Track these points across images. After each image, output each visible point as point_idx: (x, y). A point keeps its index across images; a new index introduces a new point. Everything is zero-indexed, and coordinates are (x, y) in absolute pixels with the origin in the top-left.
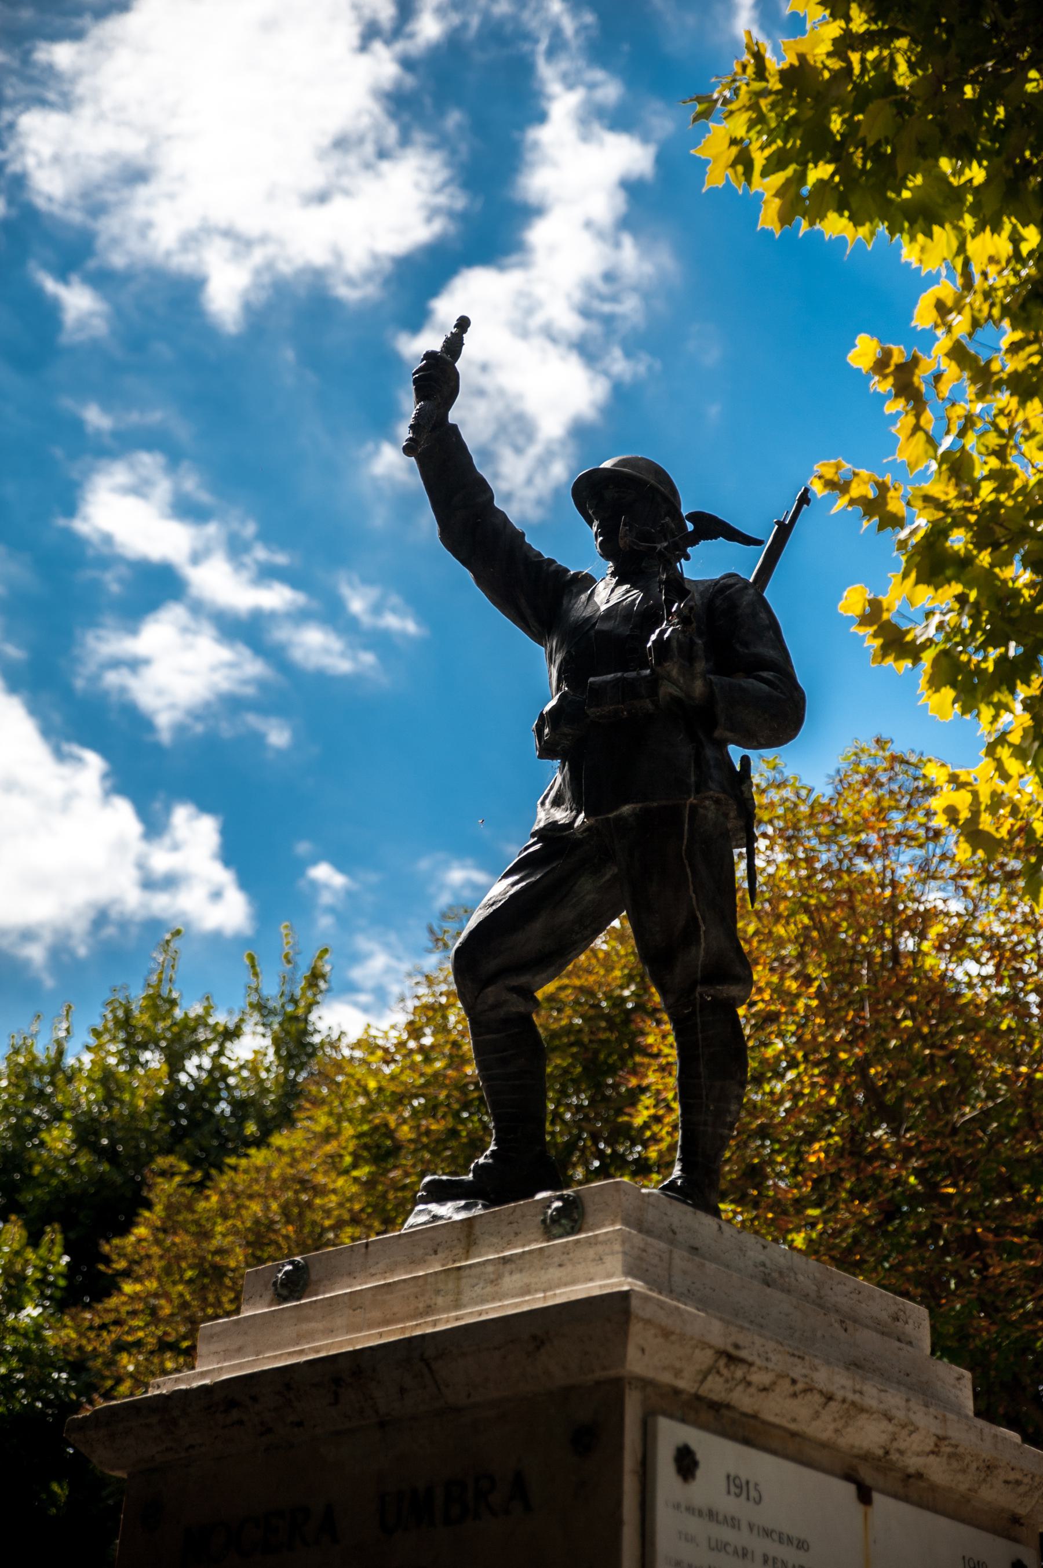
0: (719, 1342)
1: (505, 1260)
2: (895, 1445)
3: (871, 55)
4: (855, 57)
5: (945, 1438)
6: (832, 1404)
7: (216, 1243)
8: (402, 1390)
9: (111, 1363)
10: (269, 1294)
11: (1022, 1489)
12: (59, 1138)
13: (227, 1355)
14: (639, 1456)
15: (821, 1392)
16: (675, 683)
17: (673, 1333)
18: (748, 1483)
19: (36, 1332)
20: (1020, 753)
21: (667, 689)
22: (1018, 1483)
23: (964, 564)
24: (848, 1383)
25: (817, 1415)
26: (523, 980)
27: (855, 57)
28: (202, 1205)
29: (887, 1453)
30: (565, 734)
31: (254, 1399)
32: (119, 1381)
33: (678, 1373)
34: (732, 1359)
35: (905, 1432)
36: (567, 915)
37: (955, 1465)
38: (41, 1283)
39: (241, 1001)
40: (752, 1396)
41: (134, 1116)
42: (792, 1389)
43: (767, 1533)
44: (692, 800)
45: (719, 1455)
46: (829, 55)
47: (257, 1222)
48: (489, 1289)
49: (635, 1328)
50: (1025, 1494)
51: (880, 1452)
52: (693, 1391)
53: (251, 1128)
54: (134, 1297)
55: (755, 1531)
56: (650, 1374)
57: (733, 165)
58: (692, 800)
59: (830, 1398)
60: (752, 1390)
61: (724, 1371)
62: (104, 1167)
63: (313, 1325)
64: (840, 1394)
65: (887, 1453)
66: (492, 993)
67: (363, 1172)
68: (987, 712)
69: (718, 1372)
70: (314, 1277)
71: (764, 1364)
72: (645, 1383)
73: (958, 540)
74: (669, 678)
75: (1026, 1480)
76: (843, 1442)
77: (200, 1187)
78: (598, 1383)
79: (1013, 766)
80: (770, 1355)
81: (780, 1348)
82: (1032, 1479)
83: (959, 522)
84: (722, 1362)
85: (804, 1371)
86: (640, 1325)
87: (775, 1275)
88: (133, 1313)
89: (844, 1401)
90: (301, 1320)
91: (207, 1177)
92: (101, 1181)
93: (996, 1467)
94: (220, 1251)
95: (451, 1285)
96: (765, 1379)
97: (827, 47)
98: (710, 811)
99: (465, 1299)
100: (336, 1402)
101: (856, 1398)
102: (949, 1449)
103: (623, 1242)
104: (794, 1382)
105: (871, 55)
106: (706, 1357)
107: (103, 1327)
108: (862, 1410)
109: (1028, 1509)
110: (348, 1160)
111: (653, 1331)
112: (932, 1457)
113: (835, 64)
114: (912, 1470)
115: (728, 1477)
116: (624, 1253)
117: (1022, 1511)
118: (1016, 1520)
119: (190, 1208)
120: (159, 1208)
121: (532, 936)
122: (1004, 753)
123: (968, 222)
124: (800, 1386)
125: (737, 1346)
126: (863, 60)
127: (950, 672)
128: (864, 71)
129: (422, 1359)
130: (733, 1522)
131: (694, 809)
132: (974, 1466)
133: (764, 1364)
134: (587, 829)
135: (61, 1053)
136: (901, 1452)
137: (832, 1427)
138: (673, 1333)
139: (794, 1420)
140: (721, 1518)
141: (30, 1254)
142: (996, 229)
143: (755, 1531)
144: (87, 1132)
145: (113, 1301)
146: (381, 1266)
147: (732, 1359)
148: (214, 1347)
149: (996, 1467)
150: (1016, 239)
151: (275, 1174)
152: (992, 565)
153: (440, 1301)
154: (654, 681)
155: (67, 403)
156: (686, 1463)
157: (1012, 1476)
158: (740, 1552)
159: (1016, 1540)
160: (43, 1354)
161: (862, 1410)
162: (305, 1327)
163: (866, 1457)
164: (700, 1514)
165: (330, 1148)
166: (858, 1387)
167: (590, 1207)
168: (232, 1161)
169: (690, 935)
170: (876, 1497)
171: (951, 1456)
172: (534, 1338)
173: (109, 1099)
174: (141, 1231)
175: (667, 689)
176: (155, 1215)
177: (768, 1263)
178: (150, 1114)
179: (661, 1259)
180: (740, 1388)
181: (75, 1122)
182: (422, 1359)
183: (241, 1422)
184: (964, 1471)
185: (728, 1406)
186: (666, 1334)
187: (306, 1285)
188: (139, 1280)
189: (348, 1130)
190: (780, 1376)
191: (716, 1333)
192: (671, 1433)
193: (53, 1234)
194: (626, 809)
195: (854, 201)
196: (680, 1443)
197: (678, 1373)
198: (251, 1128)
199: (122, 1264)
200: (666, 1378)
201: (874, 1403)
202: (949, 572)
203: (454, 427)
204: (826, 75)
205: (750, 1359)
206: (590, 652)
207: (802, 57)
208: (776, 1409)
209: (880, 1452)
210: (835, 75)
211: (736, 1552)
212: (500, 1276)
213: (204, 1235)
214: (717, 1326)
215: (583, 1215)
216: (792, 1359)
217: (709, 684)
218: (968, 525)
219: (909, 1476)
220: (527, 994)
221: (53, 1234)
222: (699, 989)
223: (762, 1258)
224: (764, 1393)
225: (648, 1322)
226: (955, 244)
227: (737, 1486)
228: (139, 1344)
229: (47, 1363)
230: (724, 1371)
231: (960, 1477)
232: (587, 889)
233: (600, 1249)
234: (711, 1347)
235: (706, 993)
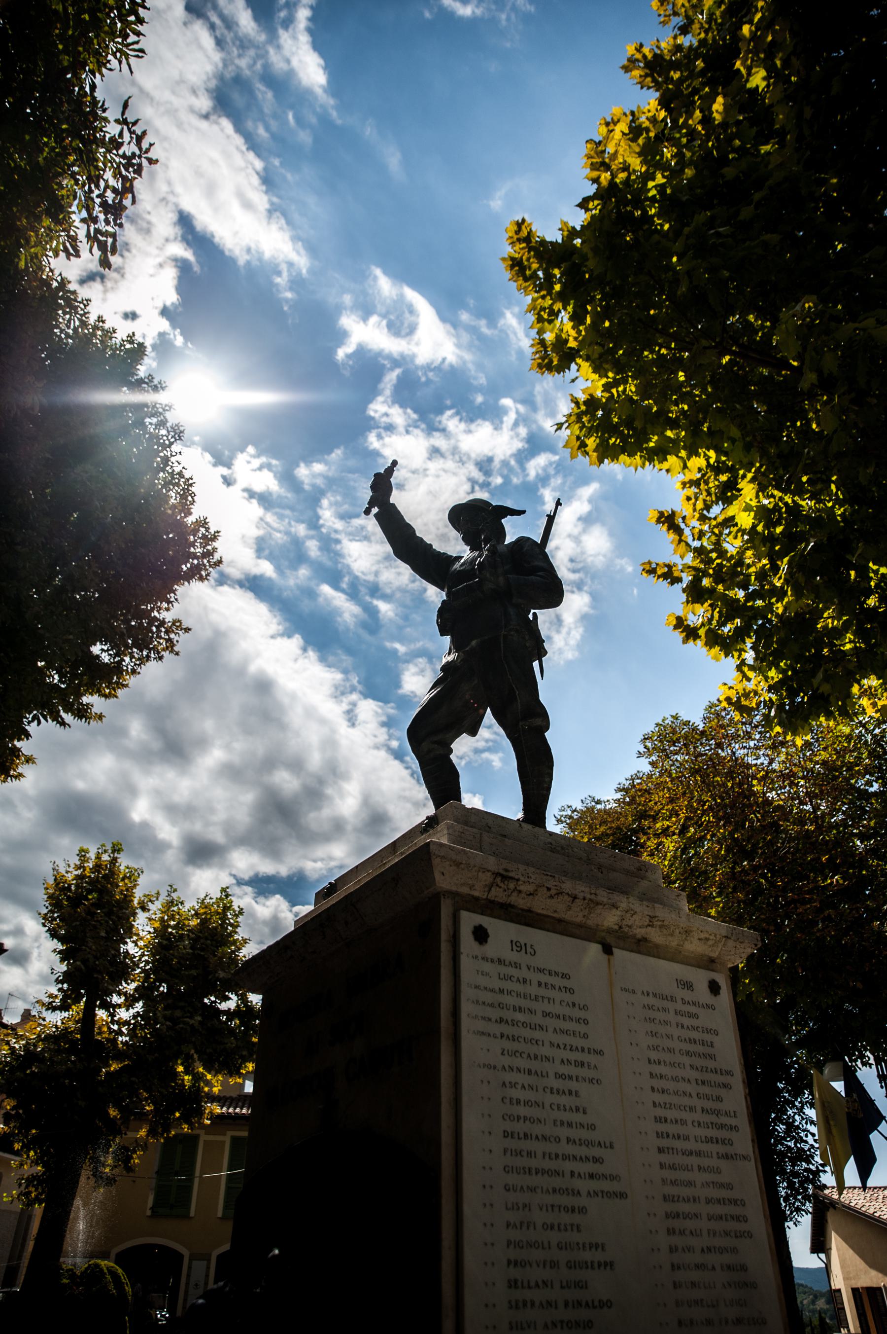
0: (495, 868)
2: (624, 922)
3: (621, 389)
4: (614, 391)
5: (655, 917)
6: (577, 900)
11: (710, 942)
14: (452, 933)
15: (568, 894)
17: (461, 863)
18: (525, 944)
20: (752, 668)
22: (707, 939)
23: (711, 592)
24: (587, 890)
25: (569, 908)
27: (614, 391)
29: (620, 927)
30: (447, 621)
33: (472, 887)
34: (504, 878)
35: (628, 915)
37: (665, 931)
40: (523, 898)
42: (549, 894)
43: (541, 971)
45: (502, 932)
46: (602, 391)
49: (436, 861)
50: (713, 945)
51: (616, 927)
52: (485, 897)
55: (532, 970)
56: (454, 889)
59: (575, 898)
60: (523, 895)
61: (502, 885)
64: (581, 895)
65: (620, 927)
68: (736, 654)
69: (497, 885)
71: (527, 879)
72: (454, 895)
73: (706, 582)
75: (711, 937)
76: (590, 922)
79: (751, 674)
80: (530, 875)
81: (538, 871)
82: (715, 936)
83: (705, 574)
84: (498, 880)
85: (555, 883)
86: (438, 860)
87: (559, 849)
89: (584, 899)
93: (691, 931)
96: (531, 888)
101: (593, 897)
102: (659, 923)
103: (448, 829)
104: (549, 889)
105: (621, 389)
106: (487, 878)
108: (598, 904)
109: (717, 953)
111: (448, 863)
112: (650, 928)
113: (607, 395)
114: (639, 936)
115: (512, 941)
116: (449, 834)
117: (714, 955)
118: (712, 961)
122: (746, 669)
123: (683, 454)
124: (553, 892)
125: (506, 870)
126: (618, 391)
127: (714, 639)
128: (619, 396)
130: (517, 966)
132: (677, 931)
133: (527, 879)
136: (630, 927)
137: (581, 914)
138: (461, 863)
139: (556, 911)
140: (507, 963)
142: (698, 455)
143: (532, 970)
147: (504, 878)
149: (691, 931)
150: (708, 459)
156: (481, 935)
157: (702, 936)
158: (521, 980)
159: (713, 970)
161: (598, 904)
163: (610, 931)
164: (492, 961)
166: (593, 891)
170: (615, 950)
171: (661, 927)
177: (553, 843)
179: (474, 837)
180: (515, 894)
184: (672, 935)
185: (511, 906)
186: (458, 864)
190: (539, 886)
191: (492, 863)
192: (469, 920)
196: (477, 924)
197: (472, 887)
200: (465, 890)
201: (605, 900)
202: (706, 597)
204: (604, 400)
205: (516, 877)
208: (541, 905)
209: (616, 927)
210: (608, 399)
211: (518, 980)
214: (492, 859)
216: (545, 877)
218: (710, 576)
219: (639, 941)
222: (521, 724)
223: (550, 840)
224: (531, 897)
225: (443, 857)
227: (516, 946)
230: (502, 885)
231: (670, 938)
234: (488, 871)
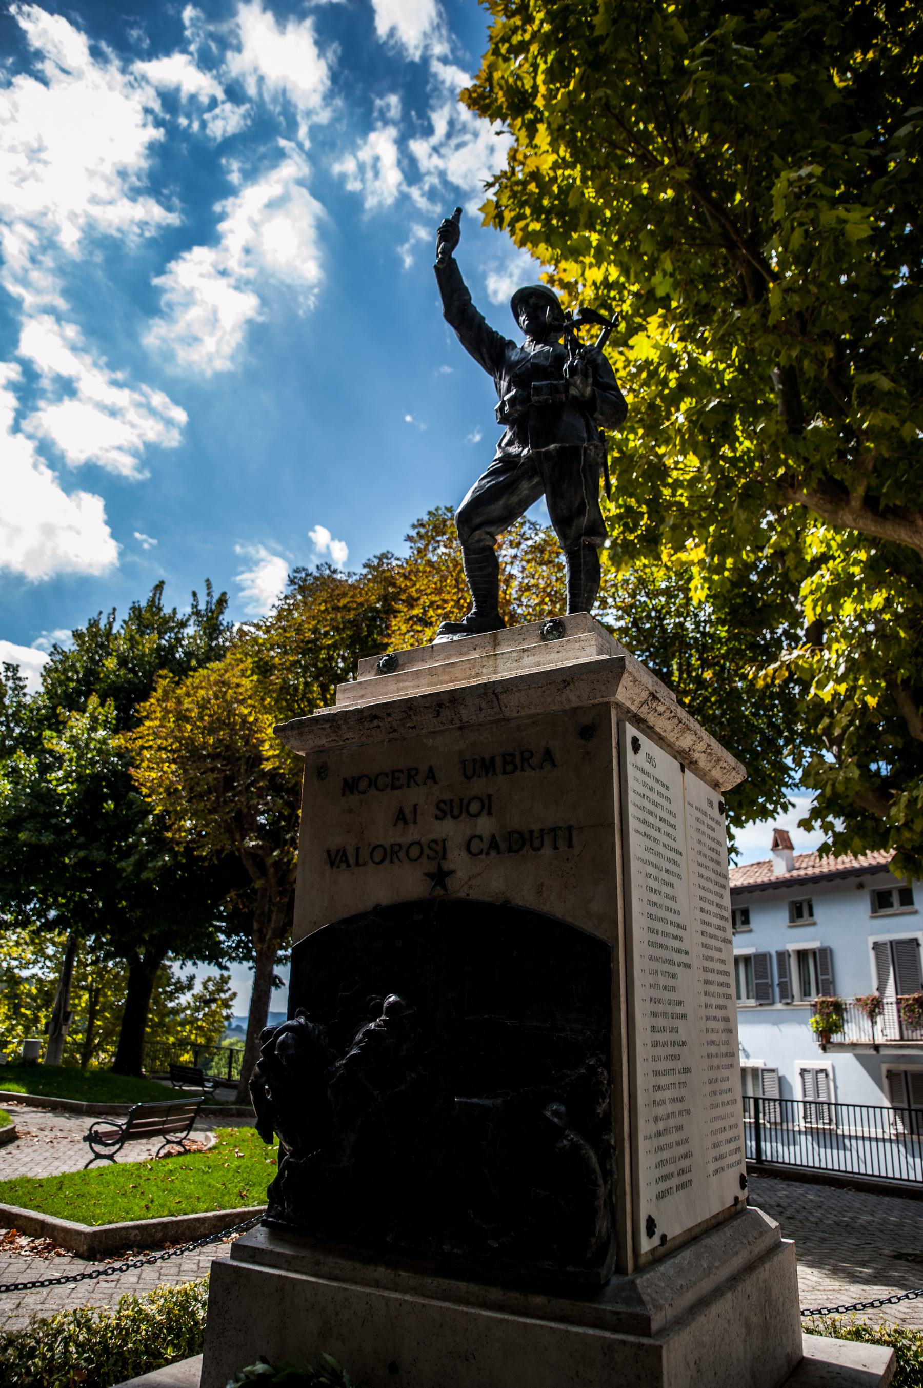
1: (524, 650)
7: (186, 706)
8: (481, 709)
9: (139, 754)
10: (373, 672)
12: (111, 663)
13: (355, 698)
16: (577, 387)
19: (104, 741)
21: (573, 391)
26: (489, 529)
28: (178, 691)
31: (389, 715)
32: (142, 761)
33: (633, 701)
36: (514, 499)
38: (106, 721)
39: (189, 610)
41: (144, 655)
43: (658, 781)
44: (585, 445)
47: (203, 699)
48: (515, 664)
53: (194, 663)
54: (149, 727)
57: (495, 217)
58: (585, 445)
62: (131, 676)
63: (407, 684)
66: (477, 534)
67: (255, 678)
70: (401, 662)
74: (575, 385)
77: (178, 684)
78: (594, 705)
88: (148, 735)
90: (398, 681)
91: (180, 679)
92: (129, 681)
94: (187, 710)
95: (491, 663)
97: (550, 164)
98: (592, 452)
99: (500, 669)
100: (438, 716)
107: (136, 739)
110: (249, 672)
113: (552, 174)
119: (174, 692)
120: (160, 691)
121: (497, 508)
129: (494, 693)
131: (585, 449)
134: (528, 457)
135: (111, 628)
141: (100, 709)
144: (123, 661)
145: (141, 729)
146: (442, 656)
148: (347, 695)
151: (212, 679)
152: (678, 371)
153: (484, 670)
154: (568, 385)
155: (373, 96)
160: (108, 750)
161: (689, 729)
162: (402, 684)
165: (241, 666)
167: (568, 626)
168: (191, 673)
169: (581, 511)
172: (564, 681)
173: (132, 648)
174: (152, 700)
175: (573, 391)
176: (159, 693)
178: (151, 655)
181: (118, 657)
182: (494, 693)
183: (379, 727)
187: (397, 665)
188: (152, 720)
189: (250, 660)
193: (110, 702)
194: (552, 447)
195: (553, 239)
198: (194, 663)
199: (145, 714)
203: (454, 260)
206: (524, 375)
207: (538, 168)
212: (521, 658)
213: (179, 702)
215: (565, 629)
217: (593, 391)
220: (493, 536)
221: (110, 702)
225: (630, 673)
226: (580, 272)
228: (151, 747)
229: (108, 753)
232: (525, 487)
233: (582, 644)
235: (585, 540)
